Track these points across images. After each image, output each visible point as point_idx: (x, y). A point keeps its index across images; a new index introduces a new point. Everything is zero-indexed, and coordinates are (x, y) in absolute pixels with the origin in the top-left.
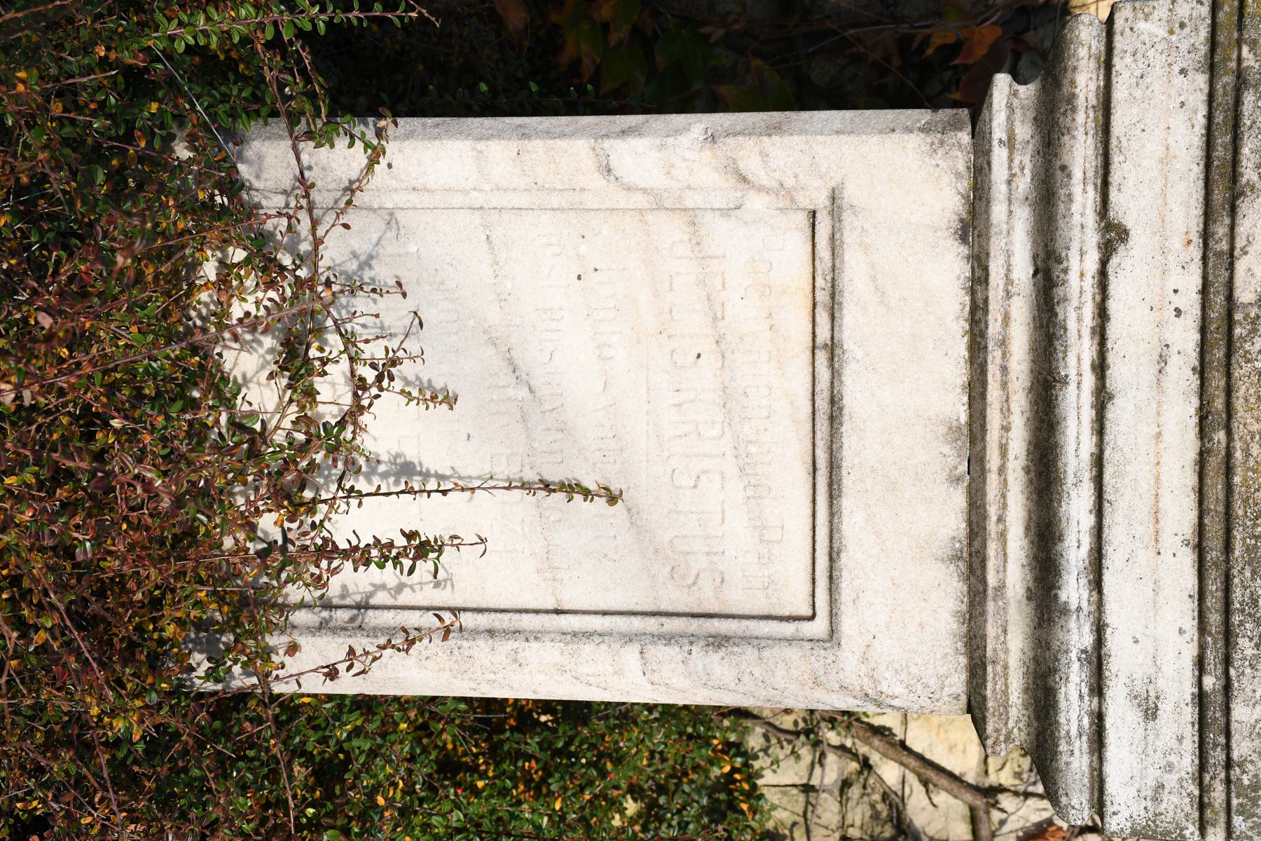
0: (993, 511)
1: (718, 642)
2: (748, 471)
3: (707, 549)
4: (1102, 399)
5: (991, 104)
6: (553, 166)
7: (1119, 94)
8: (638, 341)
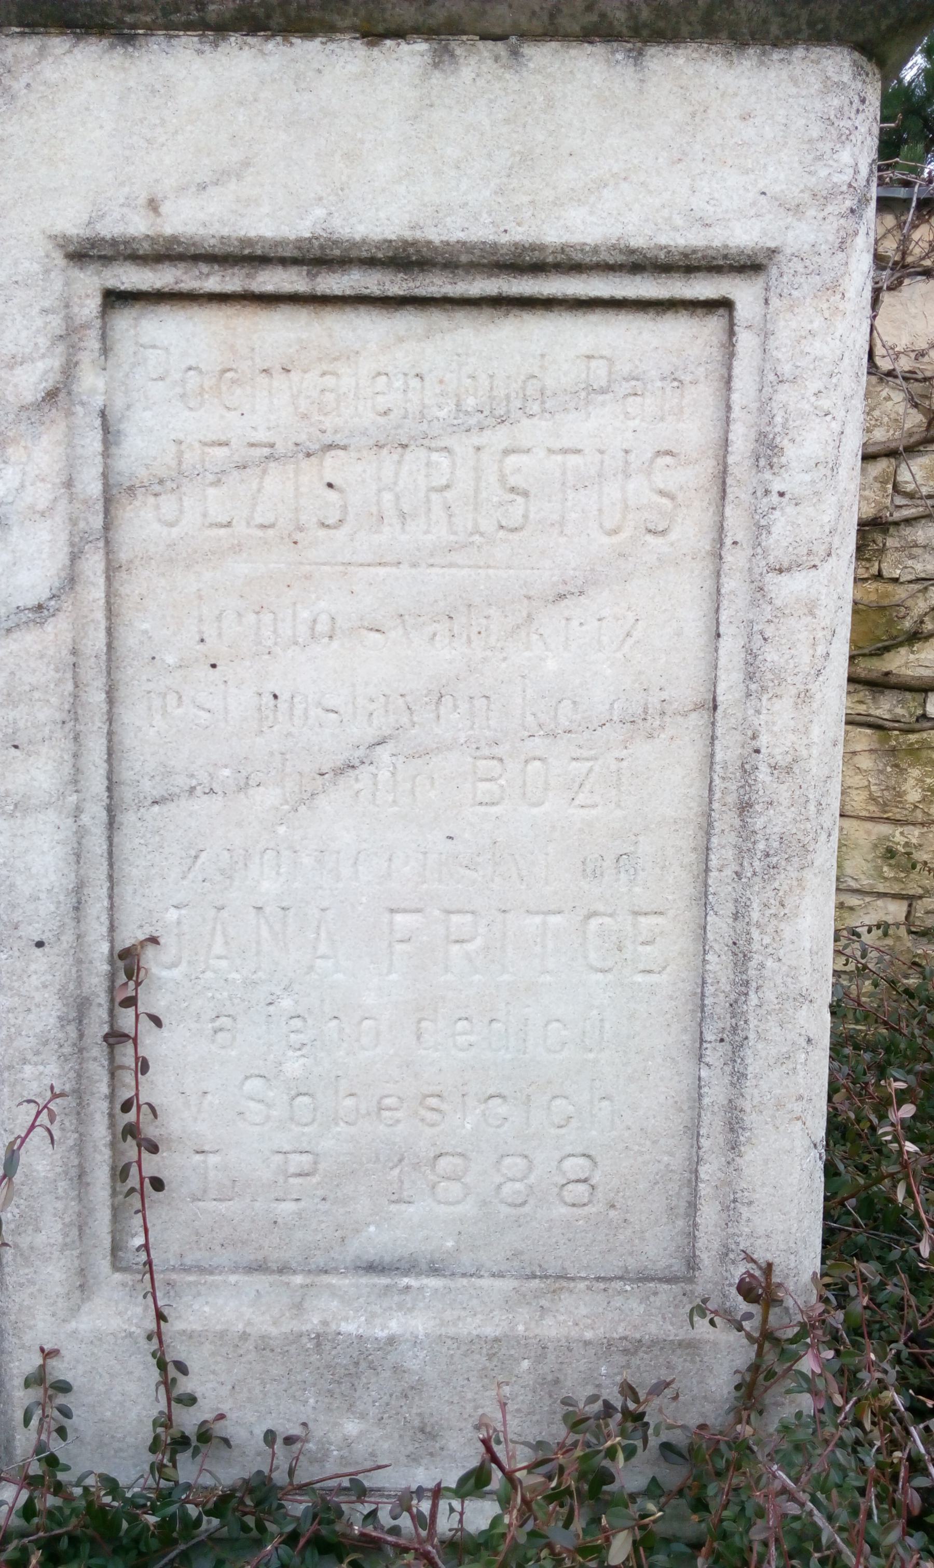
1: (767, 451)
2: (501, 411)
3: (620, 476)
6: (36, 695)
8: (308, 577)
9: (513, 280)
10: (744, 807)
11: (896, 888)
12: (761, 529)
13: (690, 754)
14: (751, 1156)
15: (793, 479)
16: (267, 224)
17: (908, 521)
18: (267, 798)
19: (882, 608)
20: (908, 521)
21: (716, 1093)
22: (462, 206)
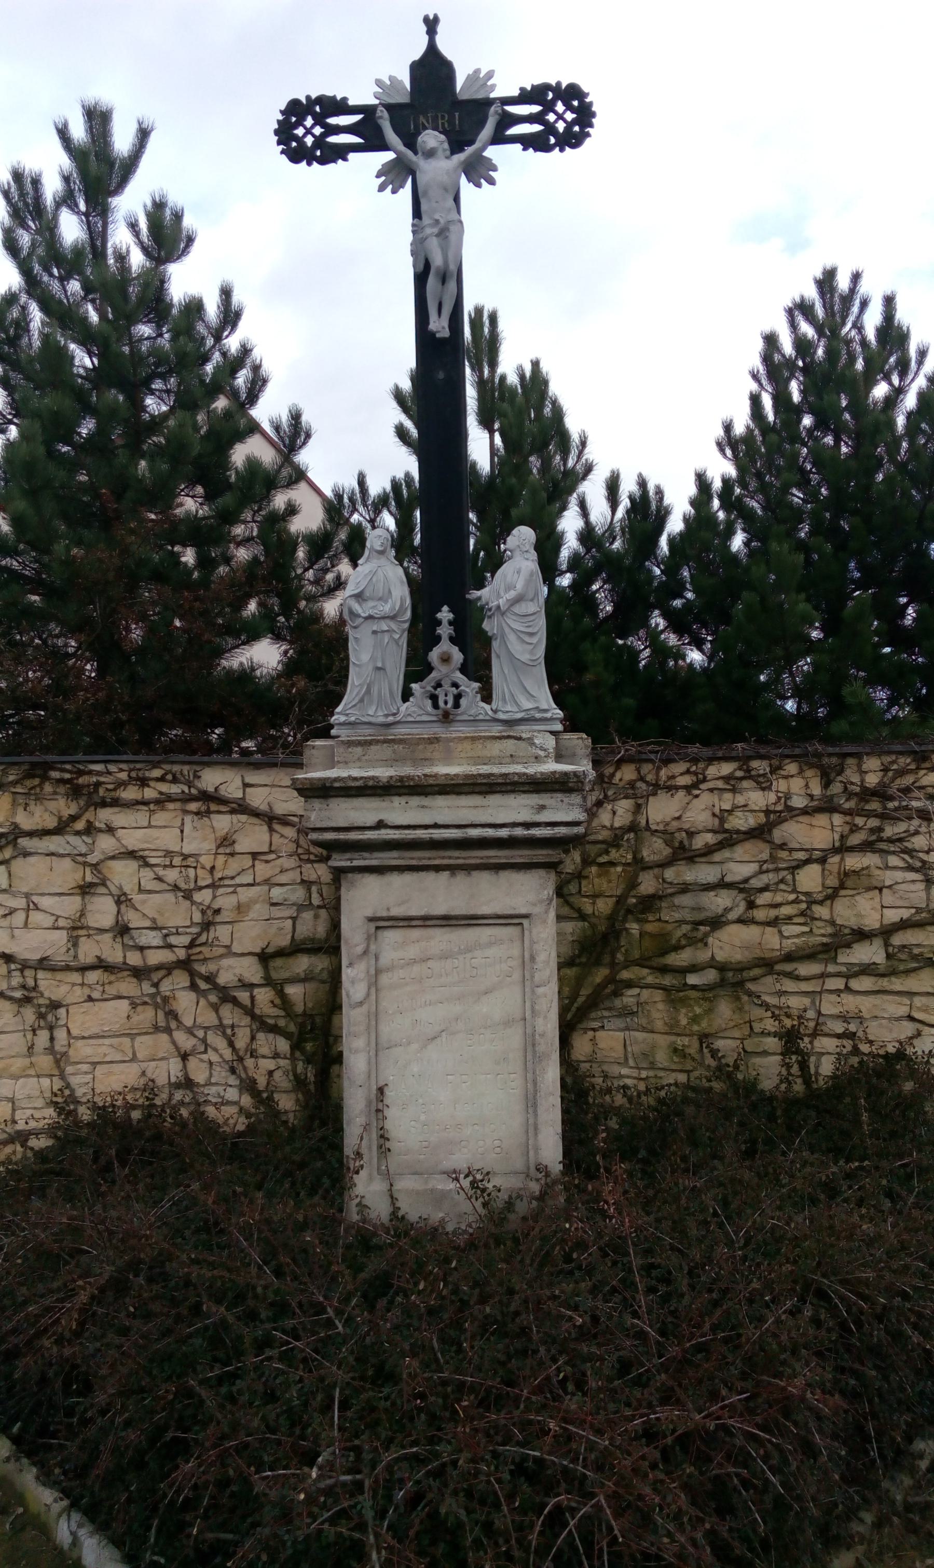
0: (479, 861)
1: (533, 959)
4: (436, 826)
5: (559, 943)
7: (334, 825)
9: (471, 920)
10: (534, 1045)
11: (679, 1067)
12: (533, 977)
13: (520, 1031)
14: (540, 1137)
15: (539, 965)
16: (413, 912)
17: (672, 895)
18: (415, 1046)
19: (662, 935)
20: (672, 895)
21: (531, 1121)
22: (460, 907)
